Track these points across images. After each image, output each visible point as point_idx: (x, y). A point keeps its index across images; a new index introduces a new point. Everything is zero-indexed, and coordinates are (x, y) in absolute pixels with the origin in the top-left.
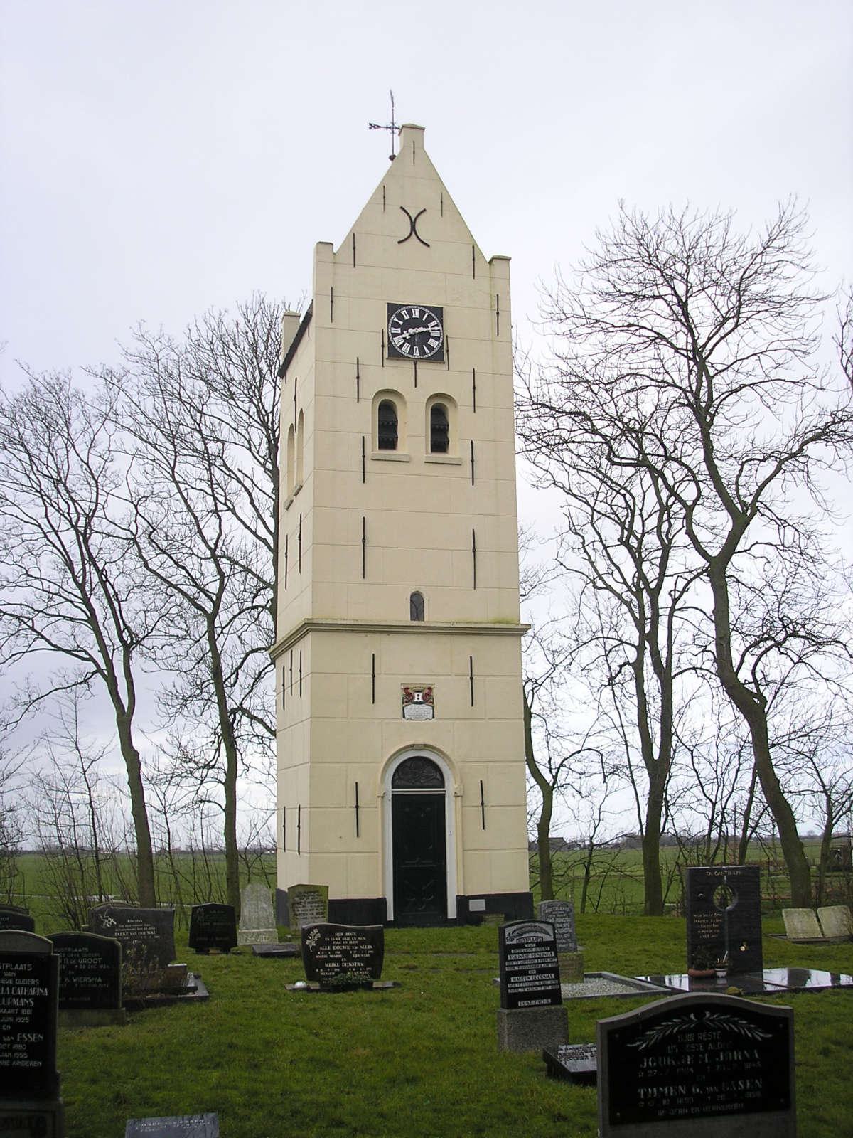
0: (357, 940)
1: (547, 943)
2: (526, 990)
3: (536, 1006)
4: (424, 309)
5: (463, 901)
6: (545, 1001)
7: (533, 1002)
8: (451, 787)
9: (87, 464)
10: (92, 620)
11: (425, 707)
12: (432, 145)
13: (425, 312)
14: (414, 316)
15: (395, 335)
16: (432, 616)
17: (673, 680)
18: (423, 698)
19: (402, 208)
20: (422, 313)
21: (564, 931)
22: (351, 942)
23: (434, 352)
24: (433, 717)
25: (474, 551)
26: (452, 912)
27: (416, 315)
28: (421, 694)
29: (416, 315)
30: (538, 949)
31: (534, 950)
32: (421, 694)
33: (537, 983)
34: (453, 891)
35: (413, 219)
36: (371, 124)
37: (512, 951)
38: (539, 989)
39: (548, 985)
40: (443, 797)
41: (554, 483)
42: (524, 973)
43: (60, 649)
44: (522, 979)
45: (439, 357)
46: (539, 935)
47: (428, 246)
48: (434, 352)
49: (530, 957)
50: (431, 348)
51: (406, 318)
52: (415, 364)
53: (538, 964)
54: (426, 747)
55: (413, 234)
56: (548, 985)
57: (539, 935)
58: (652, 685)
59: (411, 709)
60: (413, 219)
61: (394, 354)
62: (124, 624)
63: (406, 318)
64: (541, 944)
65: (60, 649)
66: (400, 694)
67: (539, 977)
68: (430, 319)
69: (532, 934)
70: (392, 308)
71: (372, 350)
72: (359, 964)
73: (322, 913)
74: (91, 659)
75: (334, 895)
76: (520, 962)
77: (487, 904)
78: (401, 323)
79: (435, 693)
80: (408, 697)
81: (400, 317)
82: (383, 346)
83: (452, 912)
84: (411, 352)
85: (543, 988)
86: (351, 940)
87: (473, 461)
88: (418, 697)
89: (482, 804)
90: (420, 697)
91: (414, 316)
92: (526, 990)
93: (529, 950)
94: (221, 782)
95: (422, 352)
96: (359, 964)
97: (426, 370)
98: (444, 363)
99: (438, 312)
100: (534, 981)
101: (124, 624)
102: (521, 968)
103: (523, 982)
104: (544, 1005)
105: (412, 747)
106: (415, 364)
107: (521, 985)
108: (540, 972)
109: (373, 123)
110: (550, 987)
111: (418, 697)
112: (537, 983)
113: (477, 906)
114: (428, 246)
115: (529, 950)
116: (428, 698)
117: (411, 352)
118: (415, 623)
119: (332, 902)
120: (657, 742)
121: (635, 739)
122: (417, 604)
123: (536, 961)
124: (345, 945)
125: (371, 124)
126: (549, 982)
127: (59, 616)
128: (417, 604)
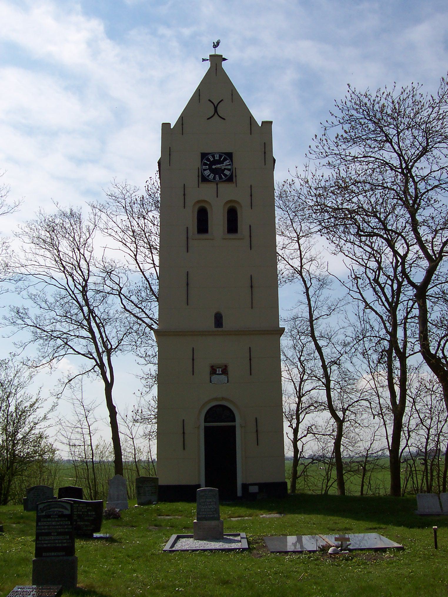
0: (86, 509)
1: (66, 516)
2: (49, 545)
3: (55, 556)
4: (221, 154)
5: (245, 487)
6: (61, 553)
7: (53, 554)
8: (238, 423)
9: (83, 255)
10: (94, 338)
11: (223, 377)
12: (224, 65)
13: (222, 156)
14: (216, 158)
15: (205, 170)
16: (227, 324)
17: (407, 359)
18: (222, 371)
19: (210, 100)
20: (220, 157)
21: (211, 506)
22: (83, 510)
23: (227, 177)
24: (228, 382)
25: (252, 287)
26: (239, 493)
27: (217, 158)
28: (220, 369)
29: (217, 158)
30: (60, 519)
31: (56, 519)
32: (220, 369)
33: (57, 541)
34: (240, 481)
35: (216, 106)
36: (203, 59)
37: (42, 520)
38: (58, 545)
39: (65, 543)
40: (234, 427)
41: (341, 251)
42: (49, 534)
43: (79, 353)
44: (47, 538)
45: (230, 179)
46: (62, 510)
47: (224, 119)
48: (227, 177)
49: (54, 523)
50: (225, 175)
51: (211, 160)
52: (217, 184)
53: (60, 528)
54: (223, 399)
55: (216, 114)
56: (65, 543)
57: (62, 510)
58: (397, 364)
59: (214, 377)
60: (216, 106)
61: (204, 179)
62: (106, 337)
63: (211, 160)
64: (62, 516)
65: (79, 353)
66: (208, 370)
67: (61, 537)
68: (225, 159)
69: (56, 509)
70: (204, 156)
71: (193, 178)
72: (87, 523)
73: (155, 493)
74: (93, 358)
75: (161, 482)
76: (46, 527)
77: (259, 489)
78: (208, 163)
79: (230, 369)
80: (213, 371)
81: (208, 160)
82: (198, 176)
83: (239, 493)
84: (214, 178)
85: (60, 545)
86: (83, 509)
87: (250, 236)
88: (219, 371)
89: (257, 431)
90: (220, 371)
91: (216, 158)
92: (49, 545)
93: (53, 520)
94: (292, 428)
95: (221, 178)
96: (87, 523)
97: (224, 187)
98: (234, 183)
99: (230, 155)
100: (54, 540)
101: (106, 337)
102: (46, 531)
103: (47, 540)
104: (59, 556)
105: (216, 399)
106: (217, 184)
107: (46, 542)
108: (60, 534)
109: (204, 58)
110: (65, 545)
111: (219, 371)
112: (57, 541)
113: (254, 489)
114: (224, 119)
115: (53, 520)
116: (225, 371)
117: (214, 178)
118: (220, 329)
119: (161, 487)
120: (398, 398)
121: (387, 394)
122: (219, 320)
123: (57, 527)
124: (79, 511)
125: (203, 59)
126: (65, 541)
127: (75, 336)
128: (219, 320)
